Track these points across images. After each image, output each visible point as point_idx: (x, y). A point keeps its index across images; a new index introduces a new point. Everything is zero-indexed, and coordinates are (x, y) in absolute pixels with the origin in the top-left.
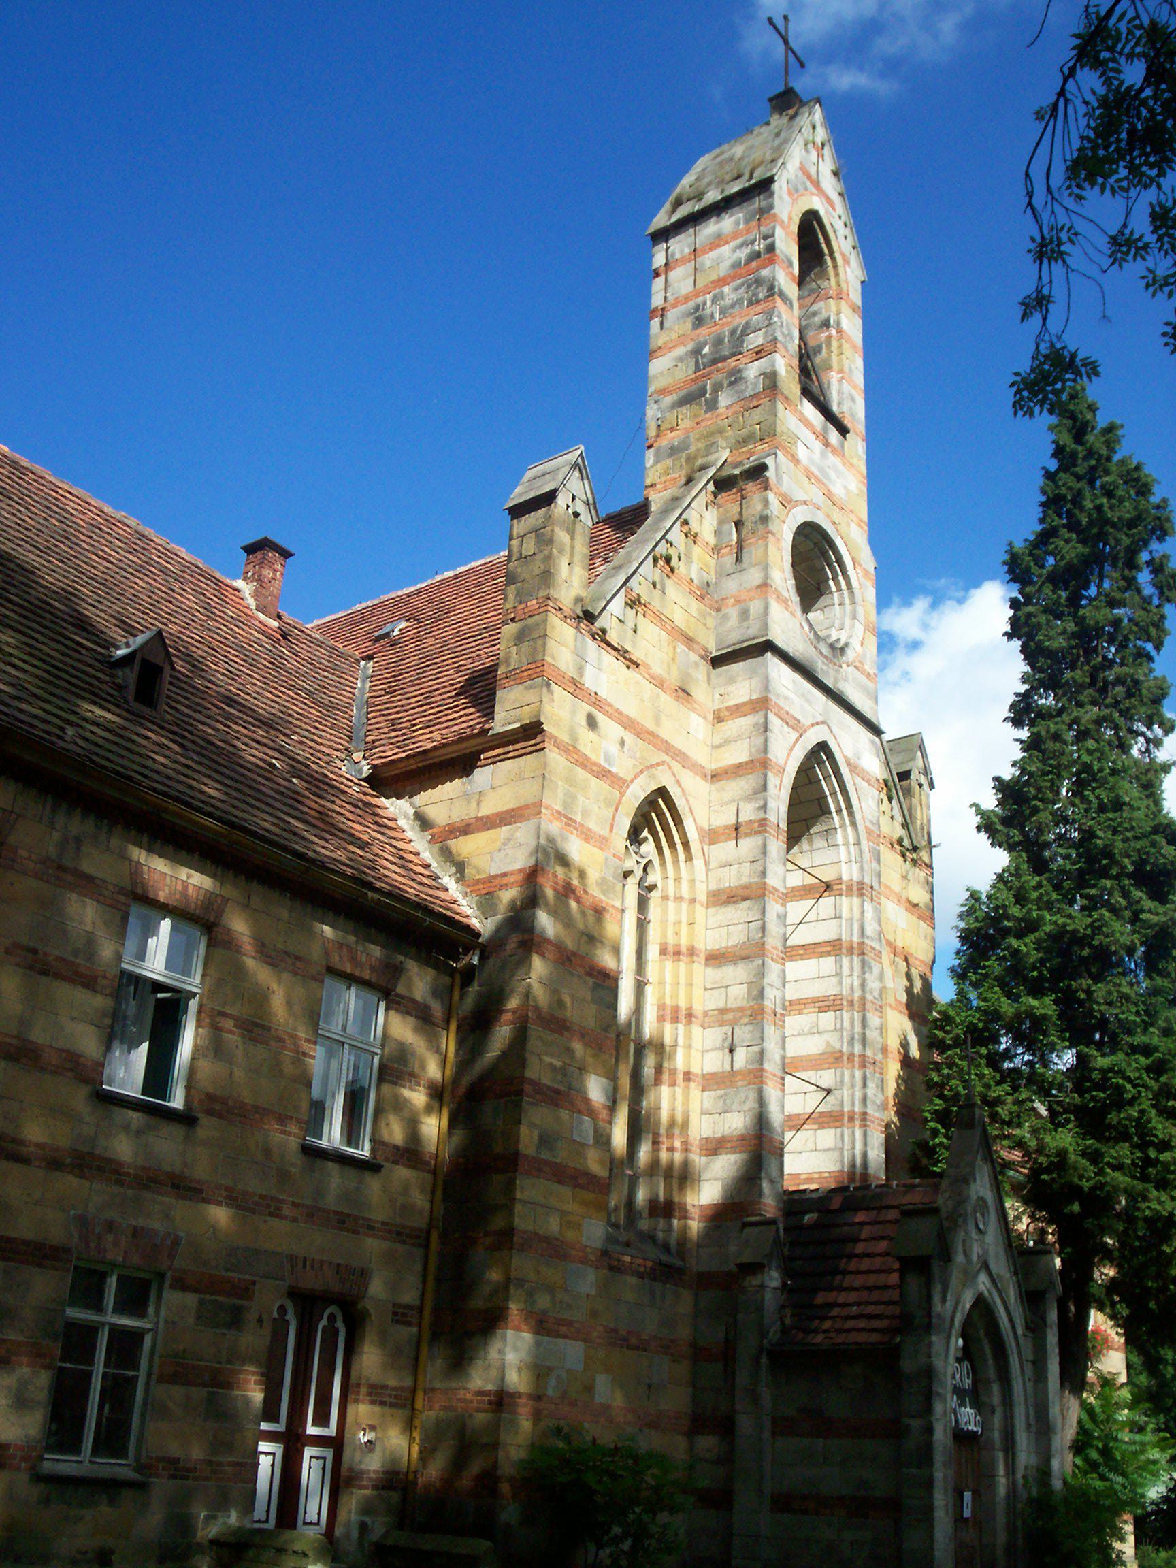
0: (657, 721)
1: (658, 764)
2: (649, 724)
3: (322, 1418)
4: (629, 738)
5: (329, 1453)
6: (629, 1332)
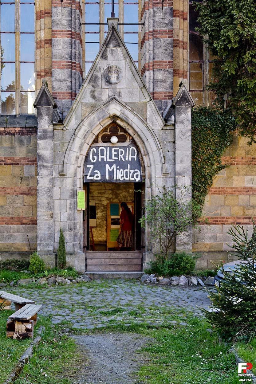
6: (5, 158)
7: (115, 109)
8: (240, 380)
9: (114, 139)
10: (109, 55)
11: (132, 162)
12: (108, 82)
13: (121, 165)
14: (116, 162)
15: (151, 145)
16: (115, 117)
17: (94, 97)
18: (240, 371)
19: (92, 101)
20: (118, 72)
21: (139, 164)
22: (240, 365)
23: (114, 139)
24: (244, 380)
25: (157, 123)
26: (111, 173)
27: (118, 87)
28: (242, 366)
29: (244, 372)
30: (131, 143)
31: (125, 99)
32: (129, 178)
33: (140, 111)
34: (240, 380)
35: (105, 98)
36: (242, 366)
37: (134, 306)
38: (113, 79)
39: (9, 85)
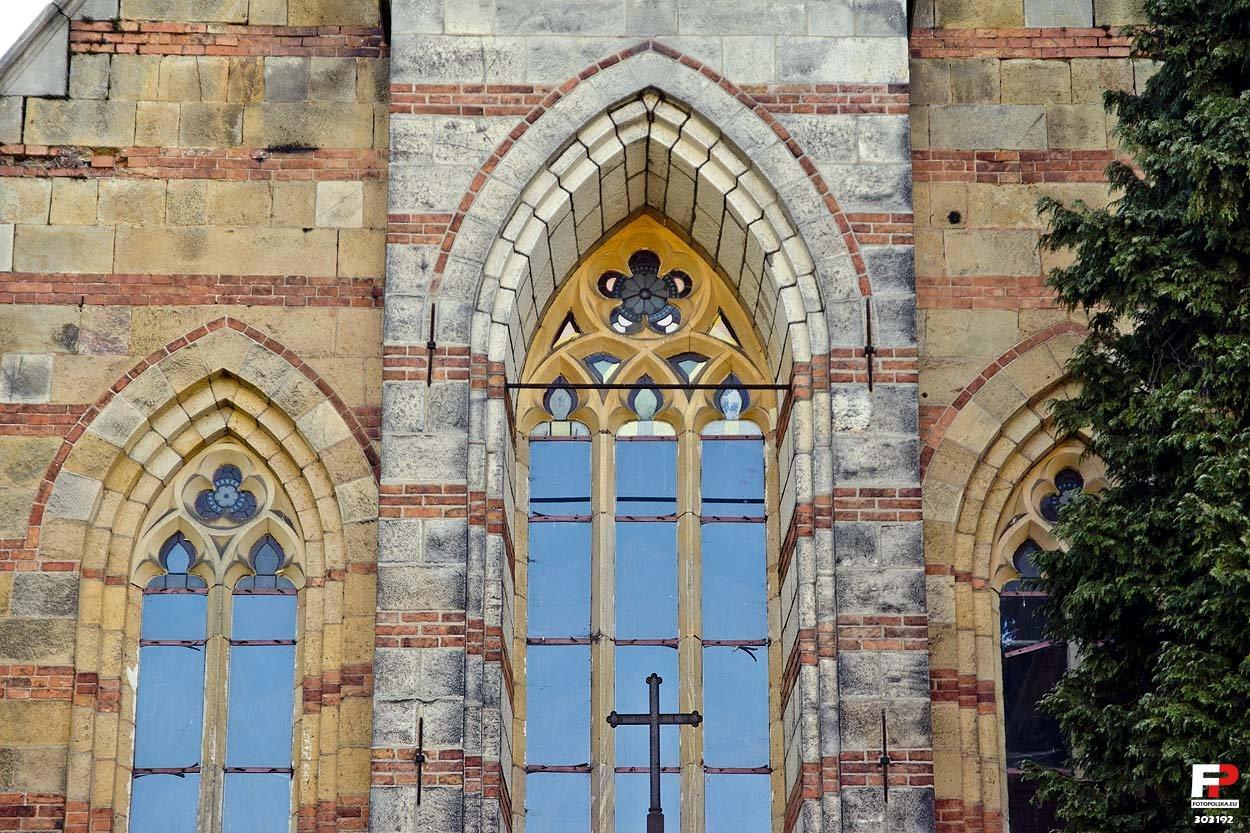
0: (193, 246)
1: (199, 333)
2: (165, 262)
4: (91, 319)
8: (1197, 821)
18: (1197, 791)
22: (1198, 770)
24: (1212, 821)
28: (1206, 775)
29: (1207, 793)
34: (1197, 821)
36: (1206, 775)
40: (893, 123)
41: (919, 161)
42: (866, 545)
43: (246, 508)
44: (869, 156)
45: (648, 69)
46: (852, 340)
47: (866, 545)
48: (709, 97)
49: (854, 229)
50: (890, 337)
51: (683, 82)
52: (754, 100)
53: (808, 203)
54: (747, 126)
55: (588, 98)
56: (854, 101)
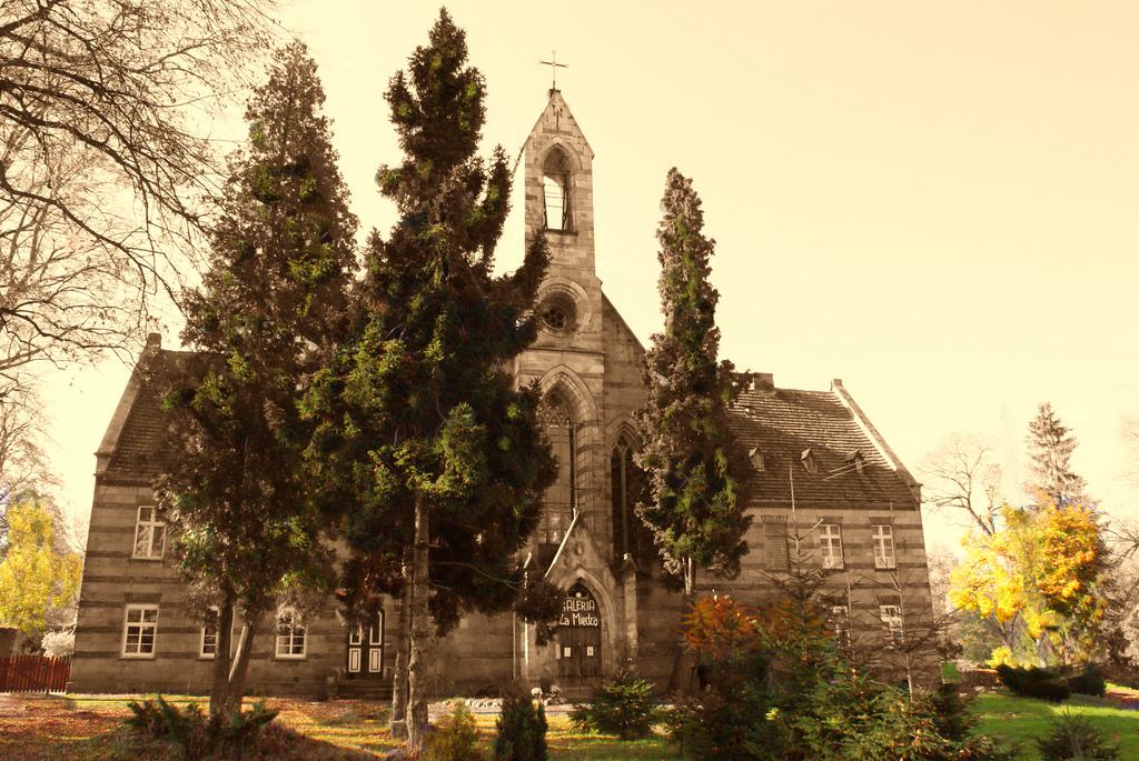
3: (376, 640)
5: (380, 650)
7: (581, 573)
9: (579, 595)
10: (576, 534)
11: (591, 612)
12: (576, 553)
13: (584, 614)
14: (580, 611)
15: (607, 600)
16: (580, 579)
17: (566, 564)
19: (564, 567)
20: (583, 547)
21: (596, 613)
23: (579, 595)
25: (612, 582)
26: (577, 620)
27: (584, 557)
30: (1045, 739)
31: (589, 566)
32: (590, 623)
33: (598, 574)
35: (574, 564)
37: (157, 117)
38: (580, 551)
39: (716, 291)
40: (601, 381)
41: (605, 384)
42: (597, 454)
43: (625, 444)
44: (597, 386)
45: (561, 369)
46: (595, 418)
47: (597, 454)
48: (572, 374)
49: (595, 399)
50: (601, 418)
51: (568, 371)
52: (578, 375)
53: (588, 394)
54: (578, 379)
55: (552, 373)
56: (595, 376)
